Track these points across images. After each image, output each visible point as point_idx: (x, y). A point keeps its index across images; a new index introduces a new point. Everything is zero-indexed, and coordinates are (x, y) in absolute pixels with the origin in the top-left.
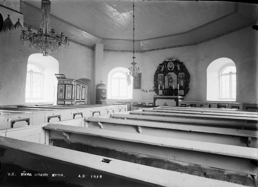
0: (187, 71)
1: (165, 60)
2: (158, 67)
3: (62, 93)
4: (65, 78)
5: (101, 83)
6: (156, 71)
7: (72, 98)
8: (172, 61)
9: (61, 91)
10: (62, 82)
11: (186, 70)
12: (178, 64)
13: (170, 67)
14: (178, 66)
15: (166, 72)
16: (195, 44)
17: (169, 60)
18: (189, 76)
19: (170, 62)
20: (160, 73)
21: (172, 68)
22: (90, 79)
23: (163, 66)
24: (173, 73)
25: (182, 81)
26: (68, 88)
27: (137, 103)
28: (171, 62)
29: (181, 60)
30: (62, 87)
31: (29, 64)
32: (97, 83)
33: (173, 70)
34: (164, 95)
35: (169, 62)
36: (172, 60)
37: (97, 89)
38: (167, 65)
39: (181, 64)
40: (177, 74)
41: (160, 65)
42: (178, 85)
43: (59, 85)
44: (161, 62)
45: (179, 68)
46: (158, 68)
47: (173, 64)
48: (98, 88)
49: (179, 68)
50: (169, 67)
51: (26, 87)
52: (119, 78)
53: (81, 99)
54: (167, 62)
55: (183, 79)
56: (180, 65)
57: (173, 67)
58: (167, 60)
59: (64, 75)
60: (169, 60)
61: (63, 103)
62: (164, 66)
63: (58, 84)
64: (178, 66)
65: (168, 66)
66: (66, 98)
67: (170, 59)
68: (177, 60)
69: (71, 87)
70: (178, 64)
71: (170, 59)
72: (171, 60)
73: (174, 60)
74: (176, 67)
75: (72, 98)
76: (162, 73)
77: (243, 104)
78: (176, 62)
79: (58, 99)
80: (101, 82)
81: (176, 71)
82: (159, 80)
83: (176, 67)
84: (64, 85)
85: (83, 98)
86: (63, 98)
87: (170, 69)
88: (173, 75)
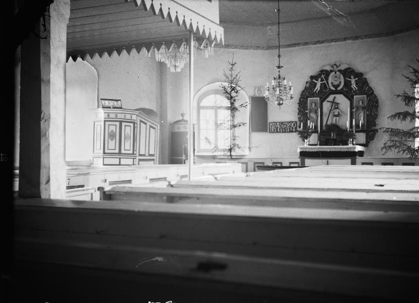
0: (373, 92)
1: (324, 66)
2: (307, 83)
3: (114, 140)
4: (121, 108)
5: (181, 118)
6: (303, 92)
7: (120, 149)
8: (340, 71)
9: (112, 136)
10: (113, 116)
11: (371, 89)
12: (352, 77)
13: (336, 83)
14: (353, 81)
15: (324, 94)
16: (393, 33)
17: (332, 69)
18: (377, 102)
19: (333, 73)
20: (313, 95)
21: (338, 85)
22: (155, 109)
23: (320, 79)
24: (342, 95)
25: (362, 114)
26: (128, 130)
27: (263, 163)
28: (337, 73)
29: (359, 67)
30: (112, 128)
31: (43, 136)
32: (171, 118)
33: (342, 89)
34: (320, 145)
35: (331, 71)
36: (339, 68)
37: (172, 133)
38: (327, 79)
39: (359, 76)
40: (350, 98)
41: (312, 77)
42: (354, 120)
43: (106, 123)
44: (314, 71)
45: (354, 86)
46: (308, 85)
47: (342, 77)
48: (176, 130)
49: (354, 86)
50: (332, 83)
51: (142, 209)
52: (216, 108)
53: (147, 154)
54: (327, 71)
55: (365, 108)
56: (357, 79)
57: (340, 82)
58: (328, 68)
59: (119, 102)
60: (332, 67)
61: (116, 161)
62: (322, 80)
63: (105, 121)
64: (353, 81)
65: (330, 80)
66: (123, 151)
67: (336, 65)
68: (349, 68)
69: (132, 127)
70: (352, 77)
71: (335, 67)
72: (337, 67)
73: (343, 67)
74: (347, 84)
75: (120, 149)
76: (317, 97)
77: (363, 156)
78: (348, 73)
79: (104, 153)
80: (182, 115)
81: (348, 94)
82: (310, 112)
83: (347, 84)
84: (118, 124)
85: (152, 153)
86: (117, 151)
87: (334, 86)
88: (342, 100)
